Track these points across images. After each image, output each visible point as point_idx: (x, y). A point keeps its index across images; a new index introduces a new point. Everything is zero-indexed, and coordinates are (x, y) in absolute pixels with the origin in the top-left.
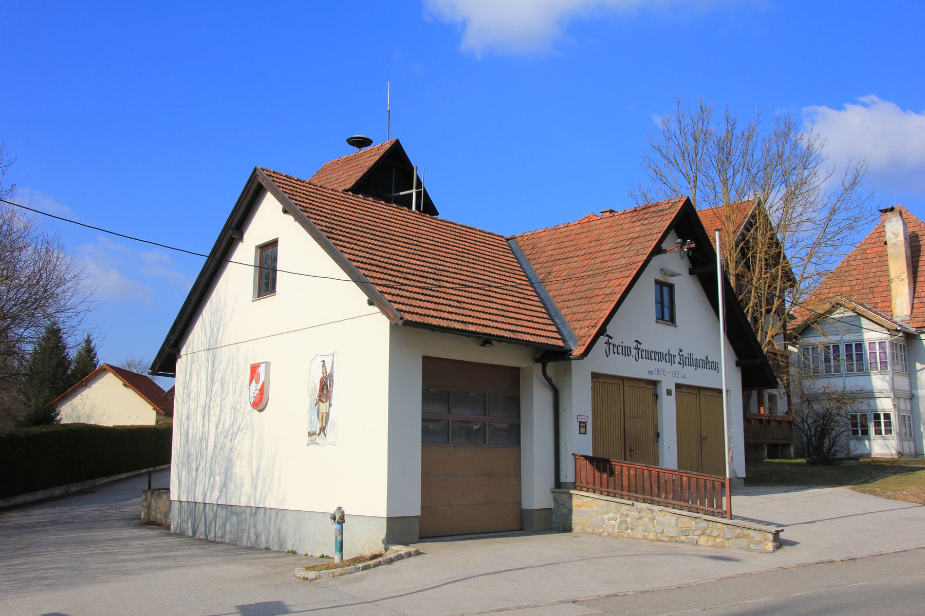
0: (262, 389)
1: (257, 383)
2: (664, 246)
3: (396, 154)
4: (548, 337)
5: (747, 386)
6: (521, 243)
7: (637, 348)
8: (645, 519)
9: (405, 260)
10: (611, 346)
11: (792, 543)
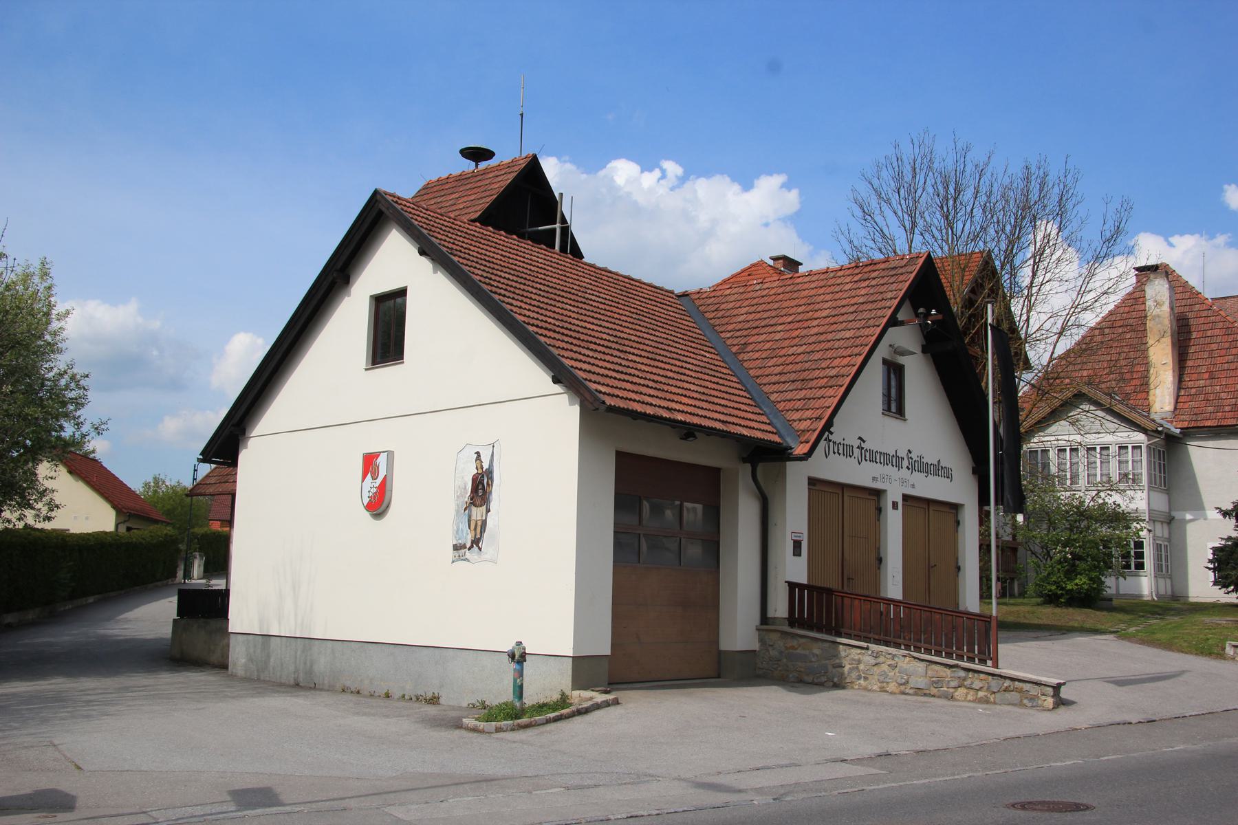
1: (375, 477)
3: (532, 174)
4: (758, 431)
6: (698, 303)
8: (885, 667)
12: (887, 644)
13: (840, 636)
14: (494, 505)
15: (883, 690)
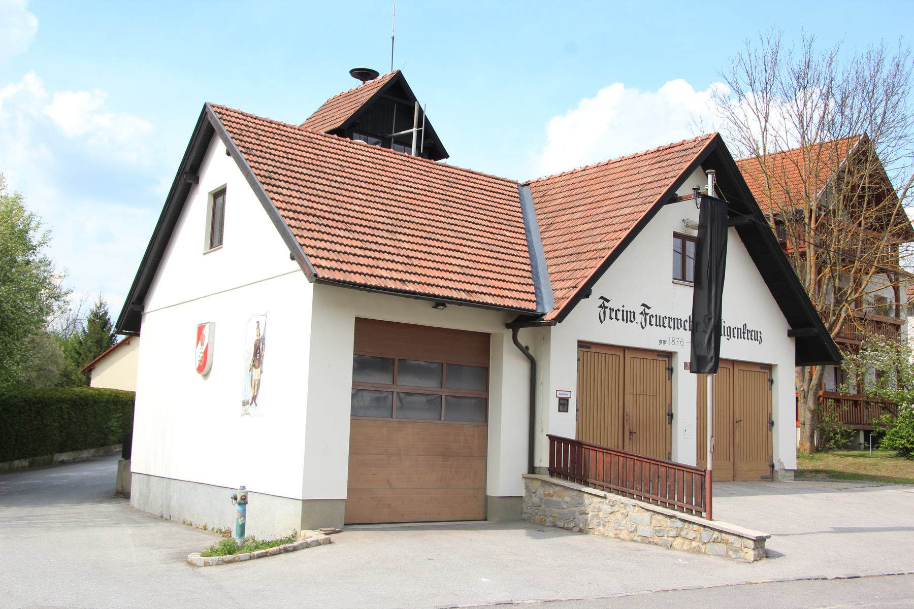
0: (205, 353)
2: (680, 192)
5: (803, 358)
7: (644, 314)
8: (619, 515)
9: (361, 209)
10: (608, 311)
11: (778, 555)
12: (623, 494)
13: (587, 484)
15: (617, 537)
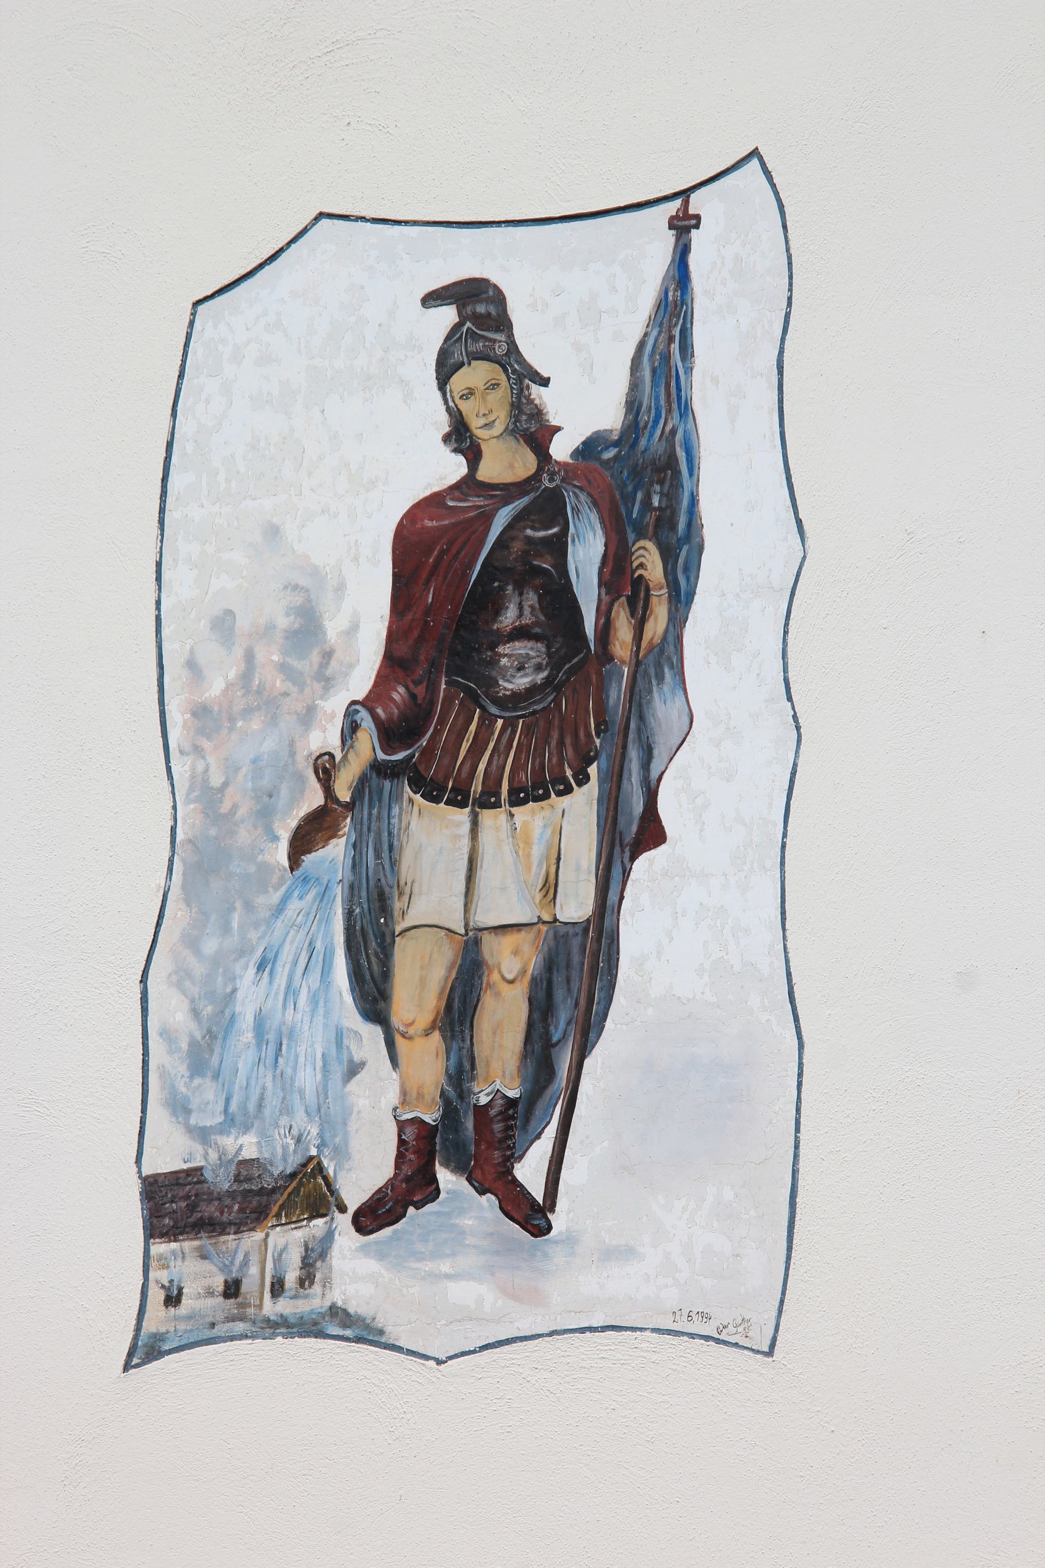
14: (710, 777)
